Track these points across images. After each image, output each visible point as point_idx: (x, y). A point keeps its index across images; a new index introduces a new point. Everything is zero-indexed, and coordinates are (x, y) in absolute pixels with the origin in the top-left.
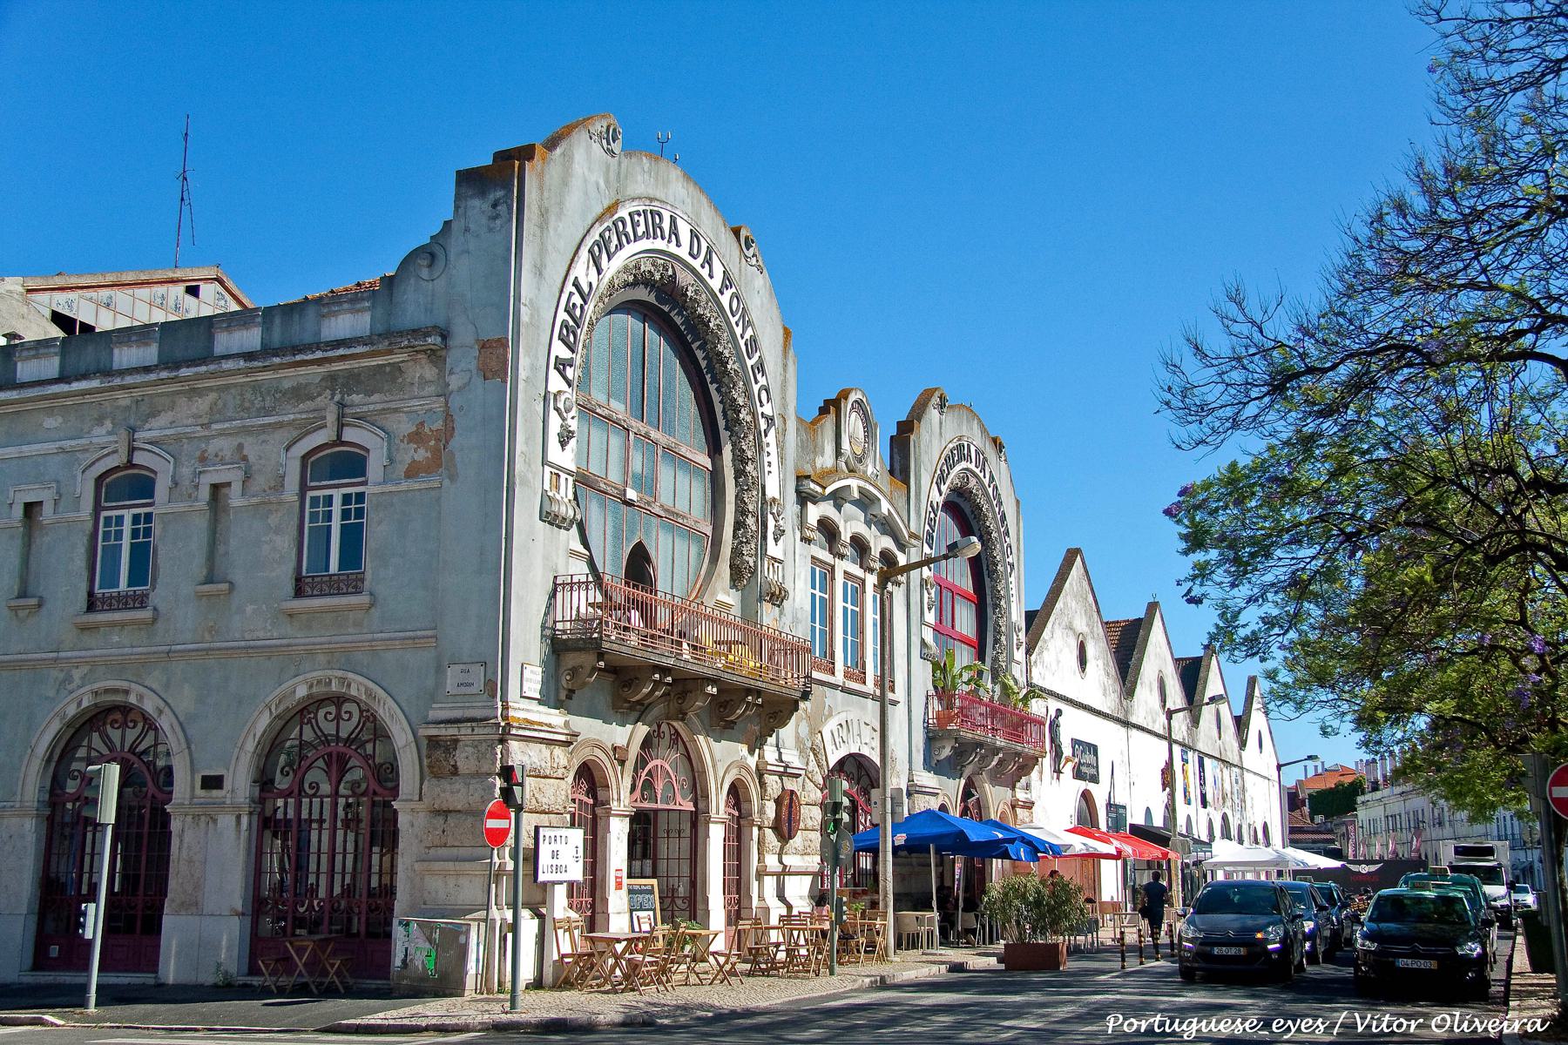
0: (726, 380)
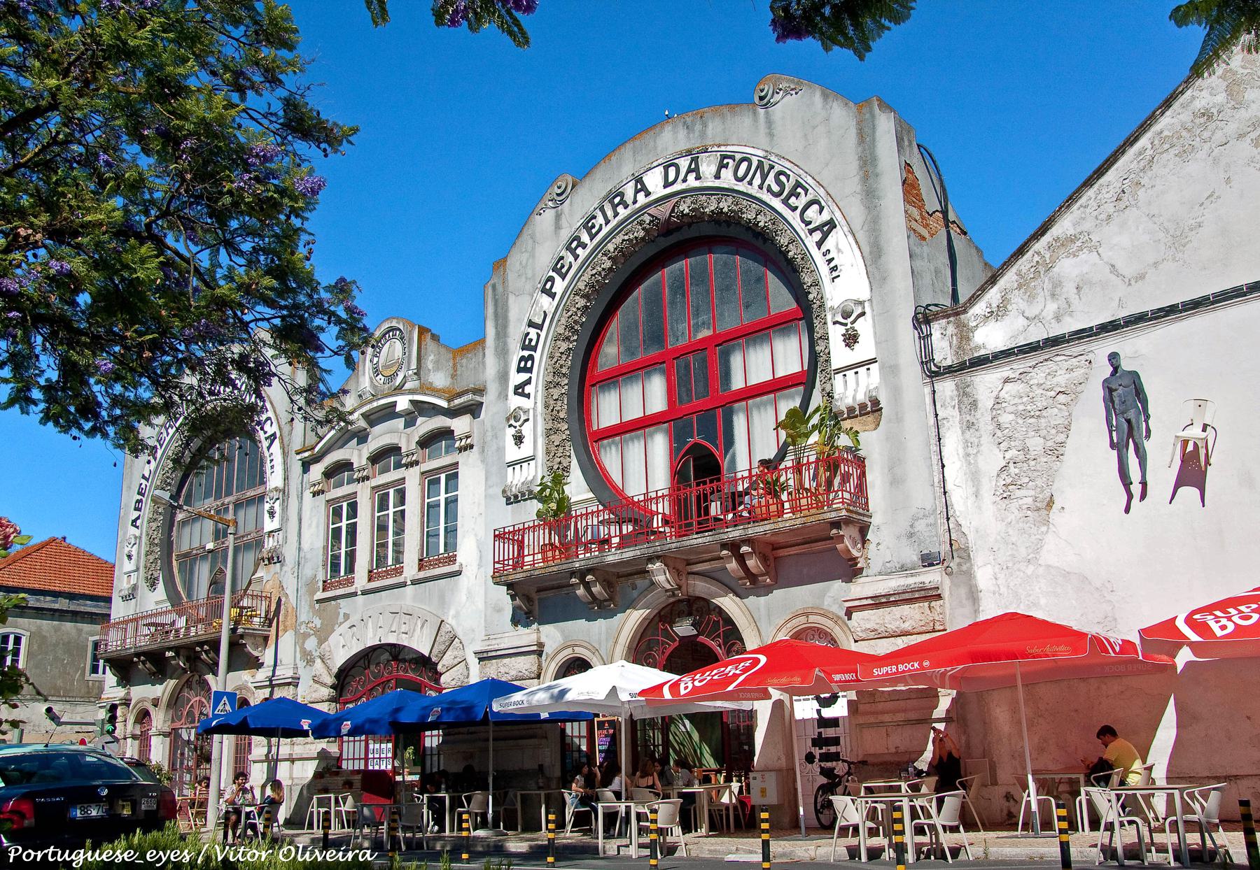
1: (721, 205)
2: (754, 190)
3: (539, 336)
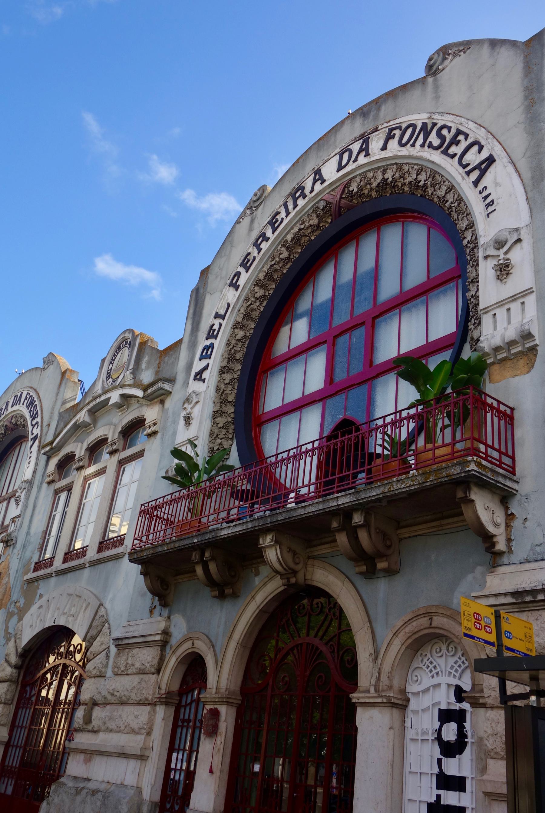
1: (386, 176)
3: (221, 325)
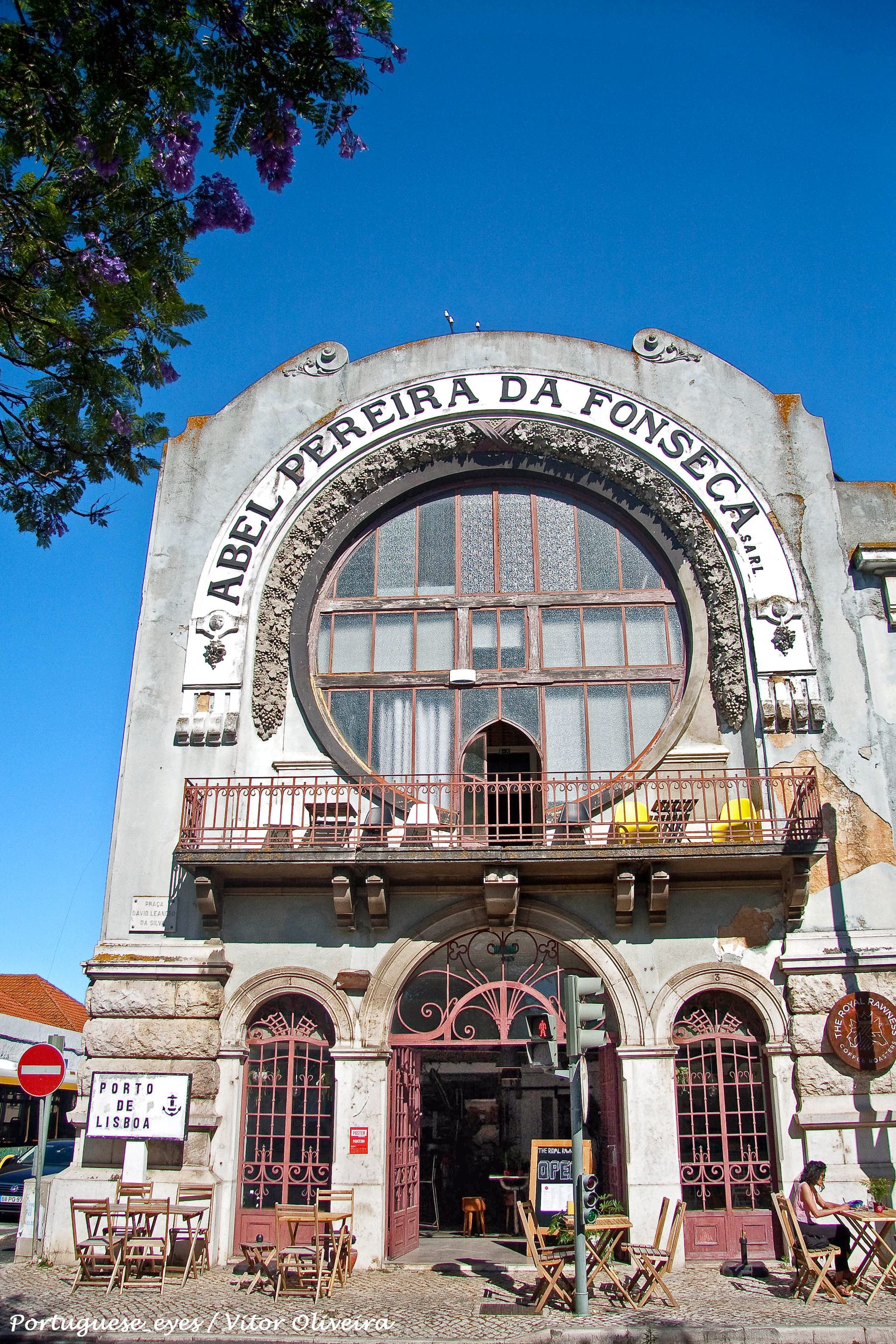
0: (648, 496)
2: (639, 439)
